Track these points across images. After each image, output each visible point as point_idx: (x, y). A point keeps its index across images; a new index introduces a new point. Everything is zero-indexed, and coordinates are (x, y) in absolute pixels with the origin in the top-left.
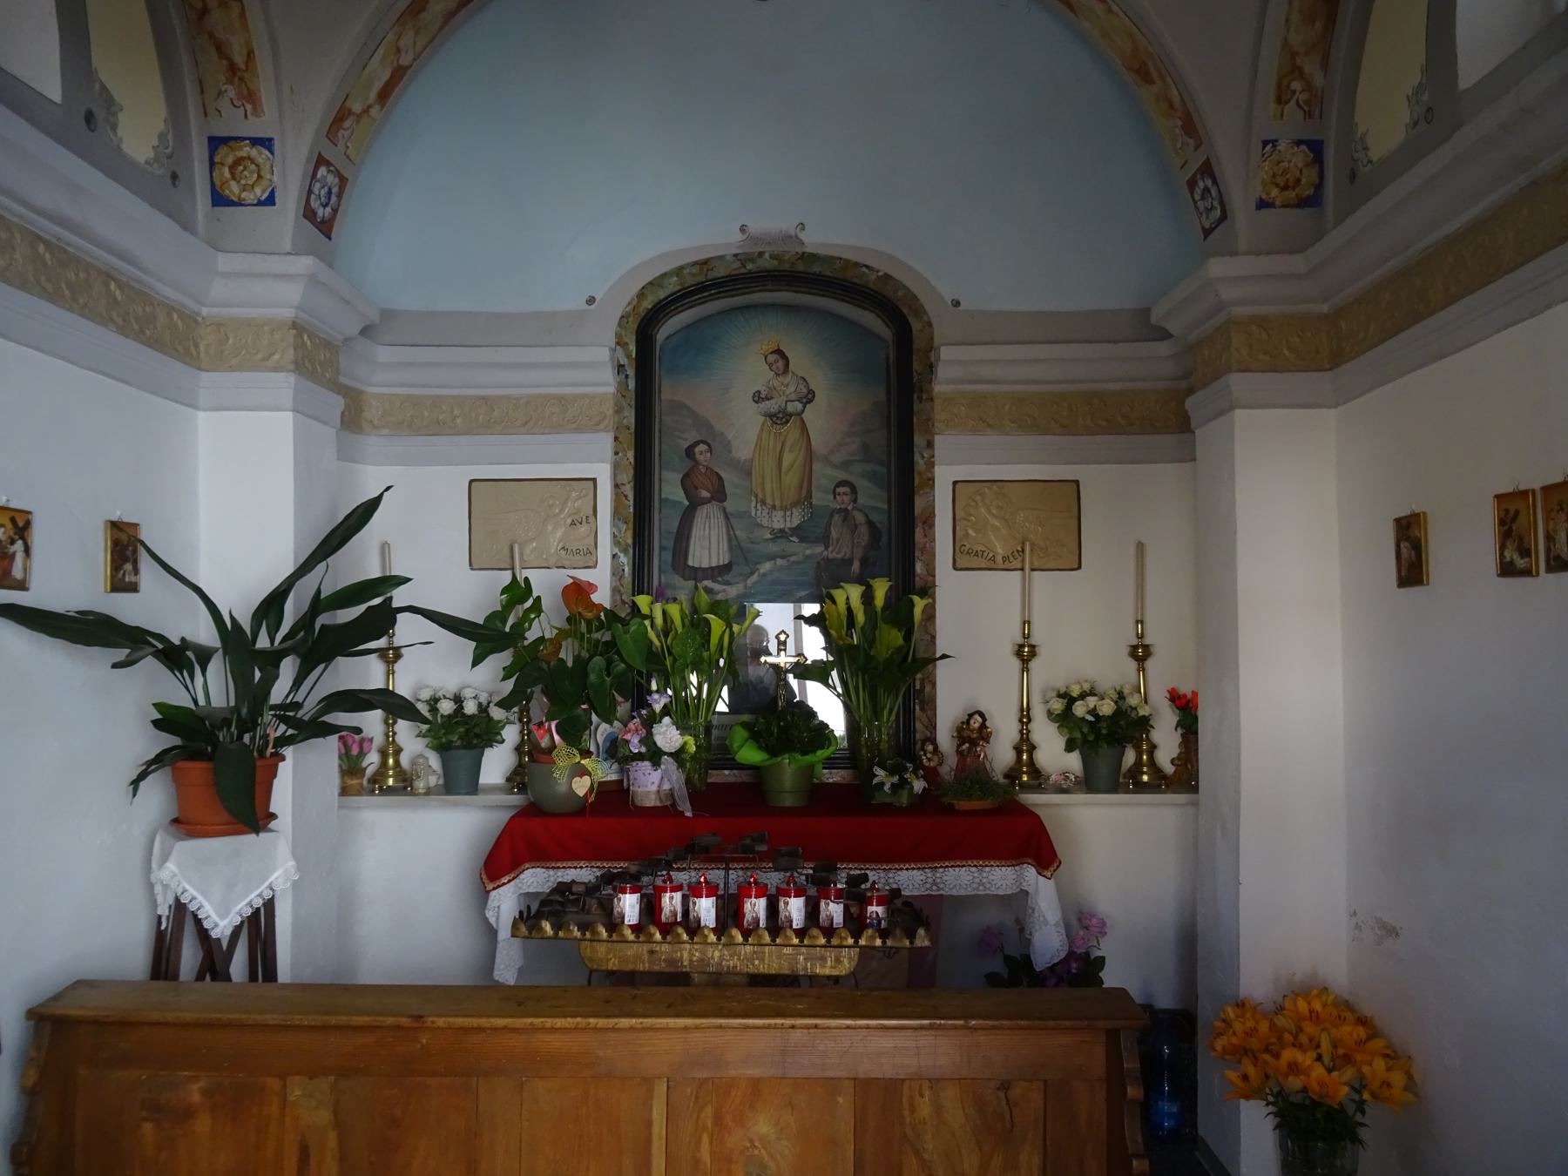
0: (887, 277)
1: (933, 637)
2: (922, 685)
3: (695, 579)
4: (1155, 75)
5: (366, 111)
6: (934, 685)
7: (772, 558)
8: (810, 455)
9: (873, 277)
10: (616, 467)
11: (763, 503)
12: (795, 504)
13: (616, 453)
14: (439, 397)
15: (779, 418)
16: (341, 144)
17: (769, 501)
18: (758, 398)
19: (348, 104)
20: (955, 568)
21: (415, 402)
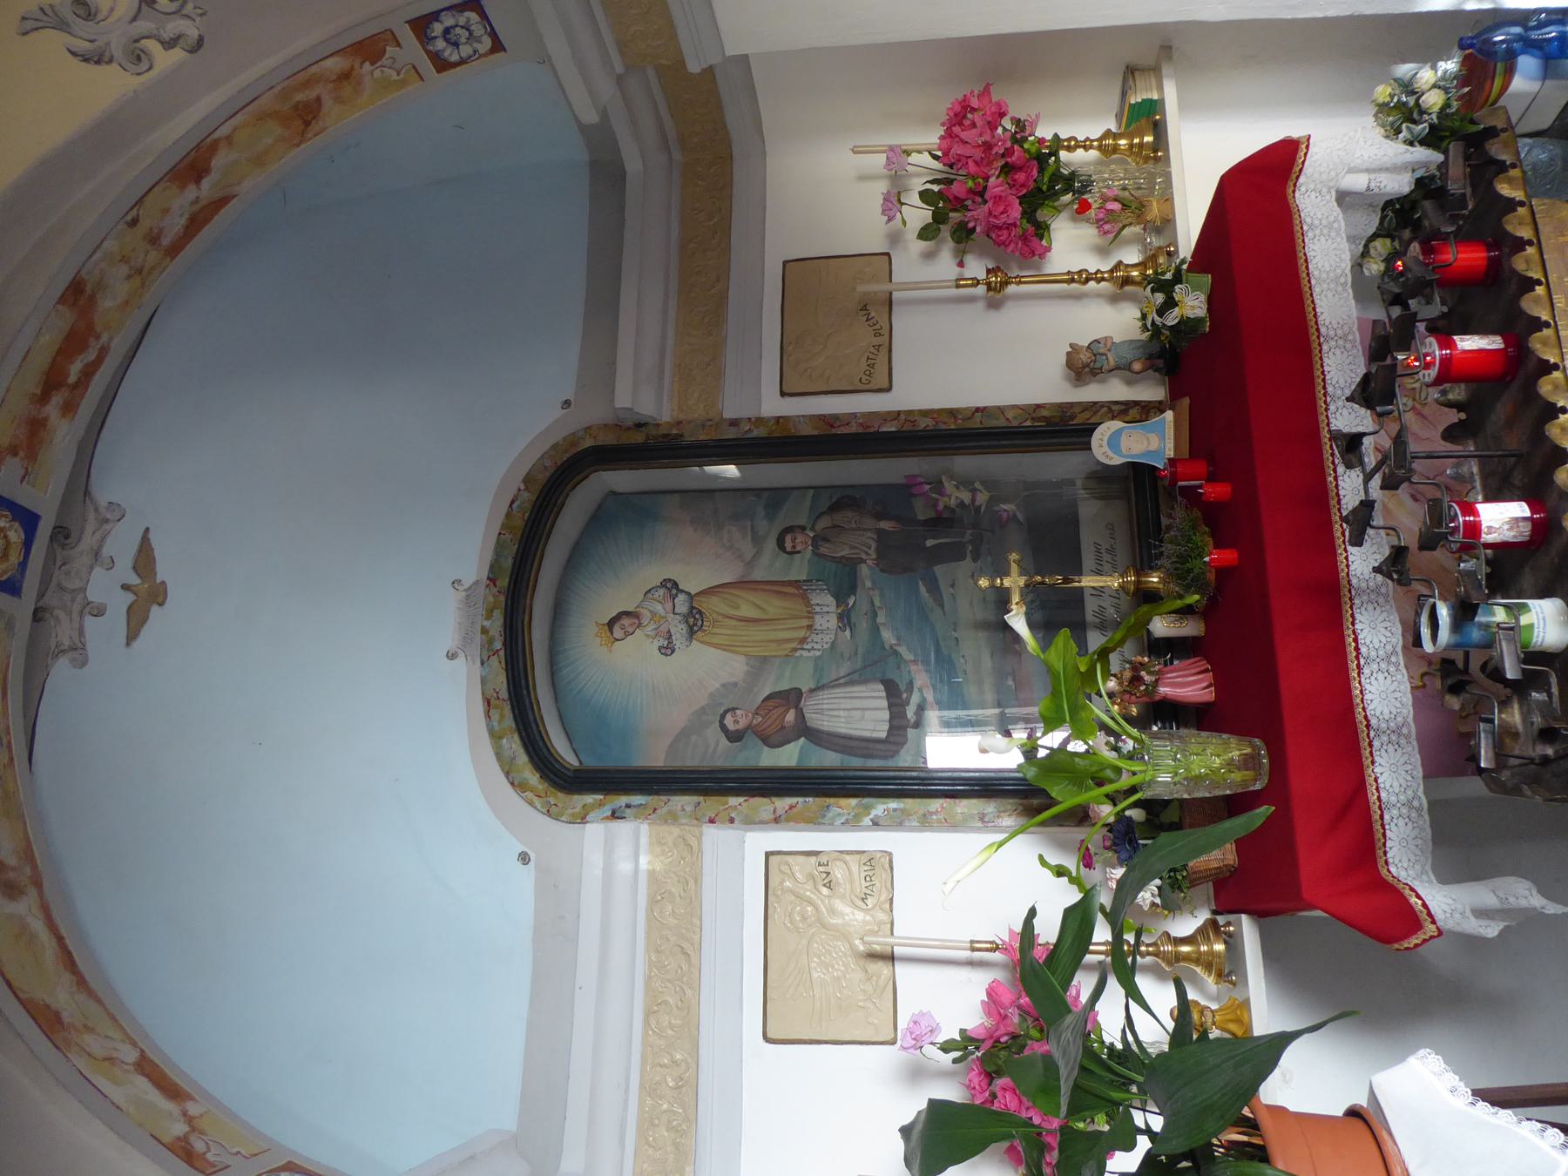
0: (527, 480)
1: (978, 409)
2: (1039, 419)
3: (904, 728)
4: (310, 94)
5: (189, 1120)
6: (1038, 406)
7: (875, 630)
8: (741, 584)
9: (526, 495)
10: (752, 822)
11: (803, 640)
12: (807, 602)
13: (732, 821)
14: (642, 1086)
15: (695, 622)
16: (228, 1160)
17: (802, 634)
18: (668, 650)
19: (166, 1140)
20: (889, 389)
21: (647, 1122)
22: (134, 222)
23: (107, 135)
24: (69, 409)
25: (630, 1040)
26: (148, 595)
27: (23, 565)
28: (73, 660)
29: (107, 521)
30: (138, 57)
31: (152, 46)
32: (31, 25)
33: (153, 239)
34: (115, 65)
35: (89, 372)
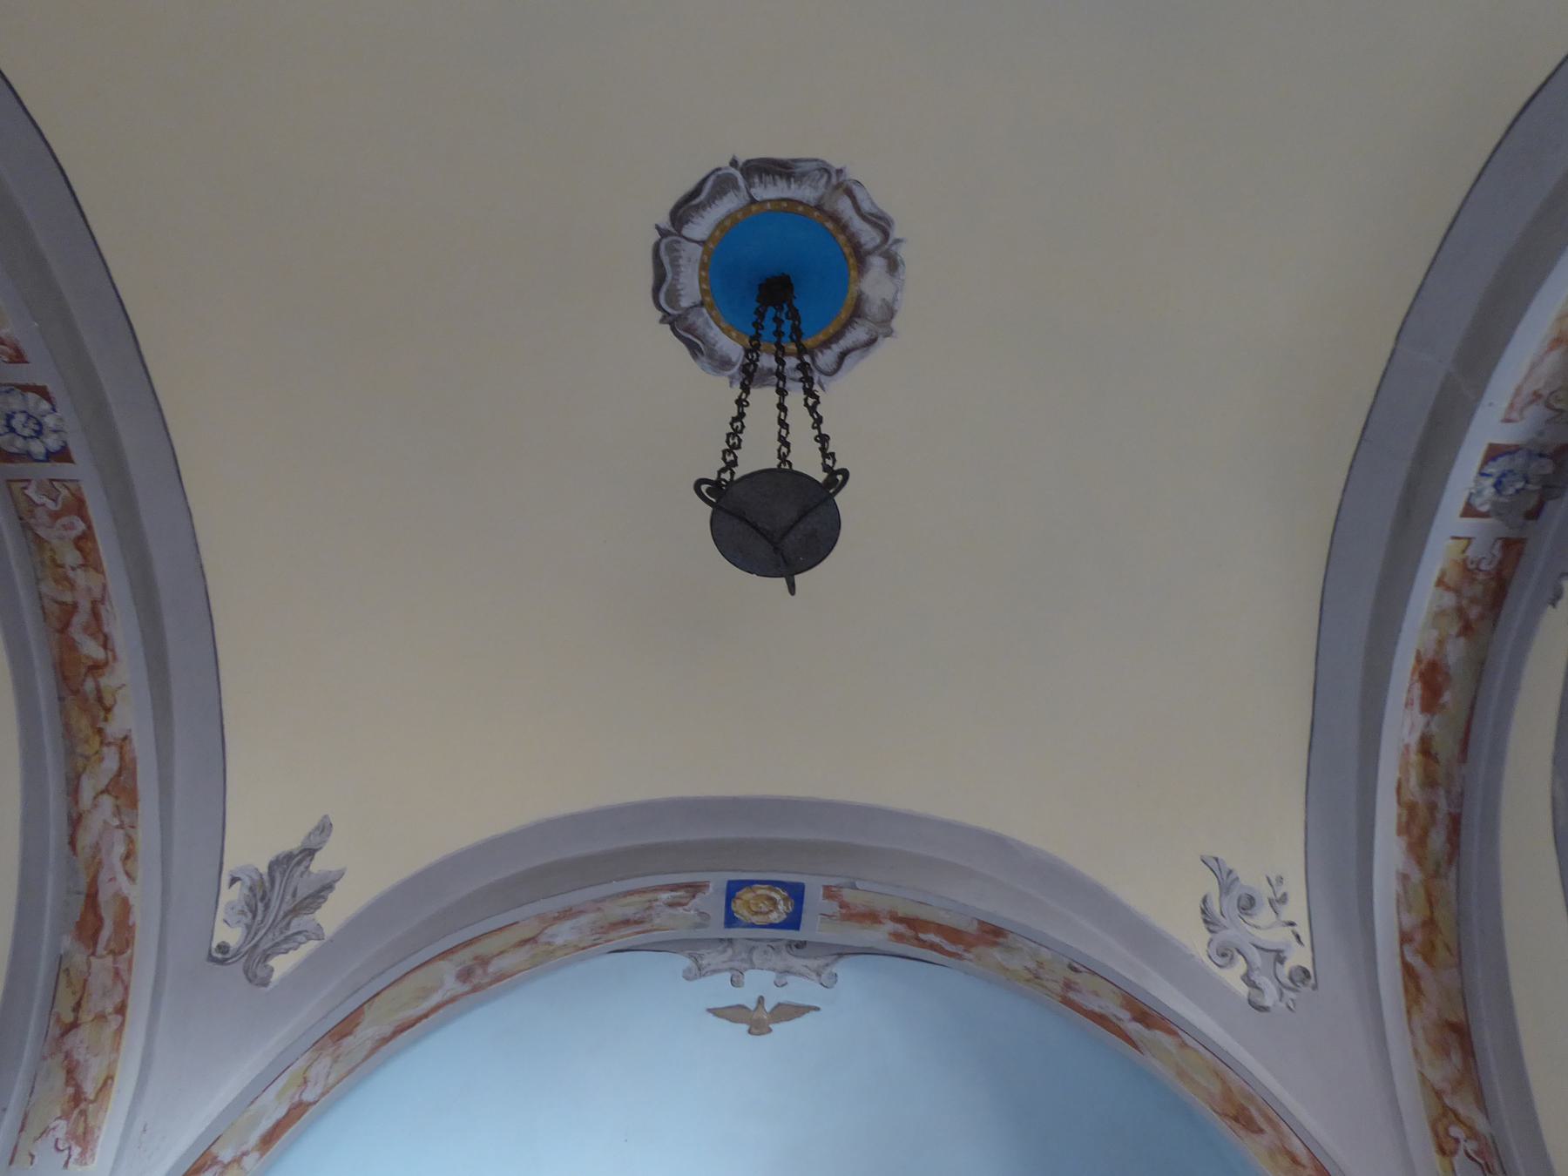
5: (237, 1160)
19: (214, 1150)
22: (1075, 970)
23: (1147, 939)
24: (898, 937)
25: (1393, 1100)
26: (757, 1020)
27: (753, 926)
28: (689, 970)
29: (819, 975)
30: (1225, 954)
31: (1240, 966)
32: (1214, 865)
33: (1068, 985)
34: (1209, 936)
35: (933, 947)
